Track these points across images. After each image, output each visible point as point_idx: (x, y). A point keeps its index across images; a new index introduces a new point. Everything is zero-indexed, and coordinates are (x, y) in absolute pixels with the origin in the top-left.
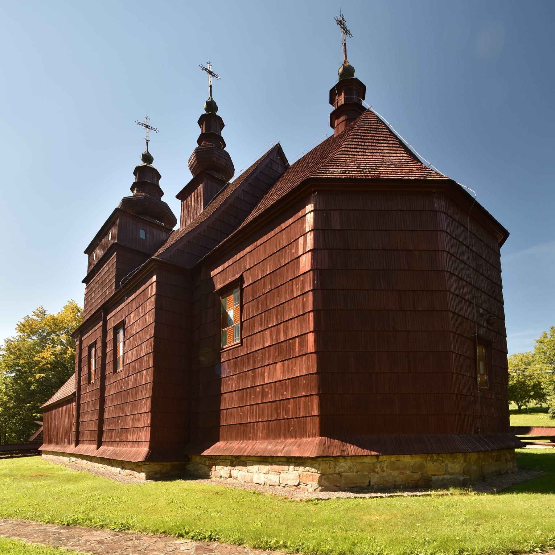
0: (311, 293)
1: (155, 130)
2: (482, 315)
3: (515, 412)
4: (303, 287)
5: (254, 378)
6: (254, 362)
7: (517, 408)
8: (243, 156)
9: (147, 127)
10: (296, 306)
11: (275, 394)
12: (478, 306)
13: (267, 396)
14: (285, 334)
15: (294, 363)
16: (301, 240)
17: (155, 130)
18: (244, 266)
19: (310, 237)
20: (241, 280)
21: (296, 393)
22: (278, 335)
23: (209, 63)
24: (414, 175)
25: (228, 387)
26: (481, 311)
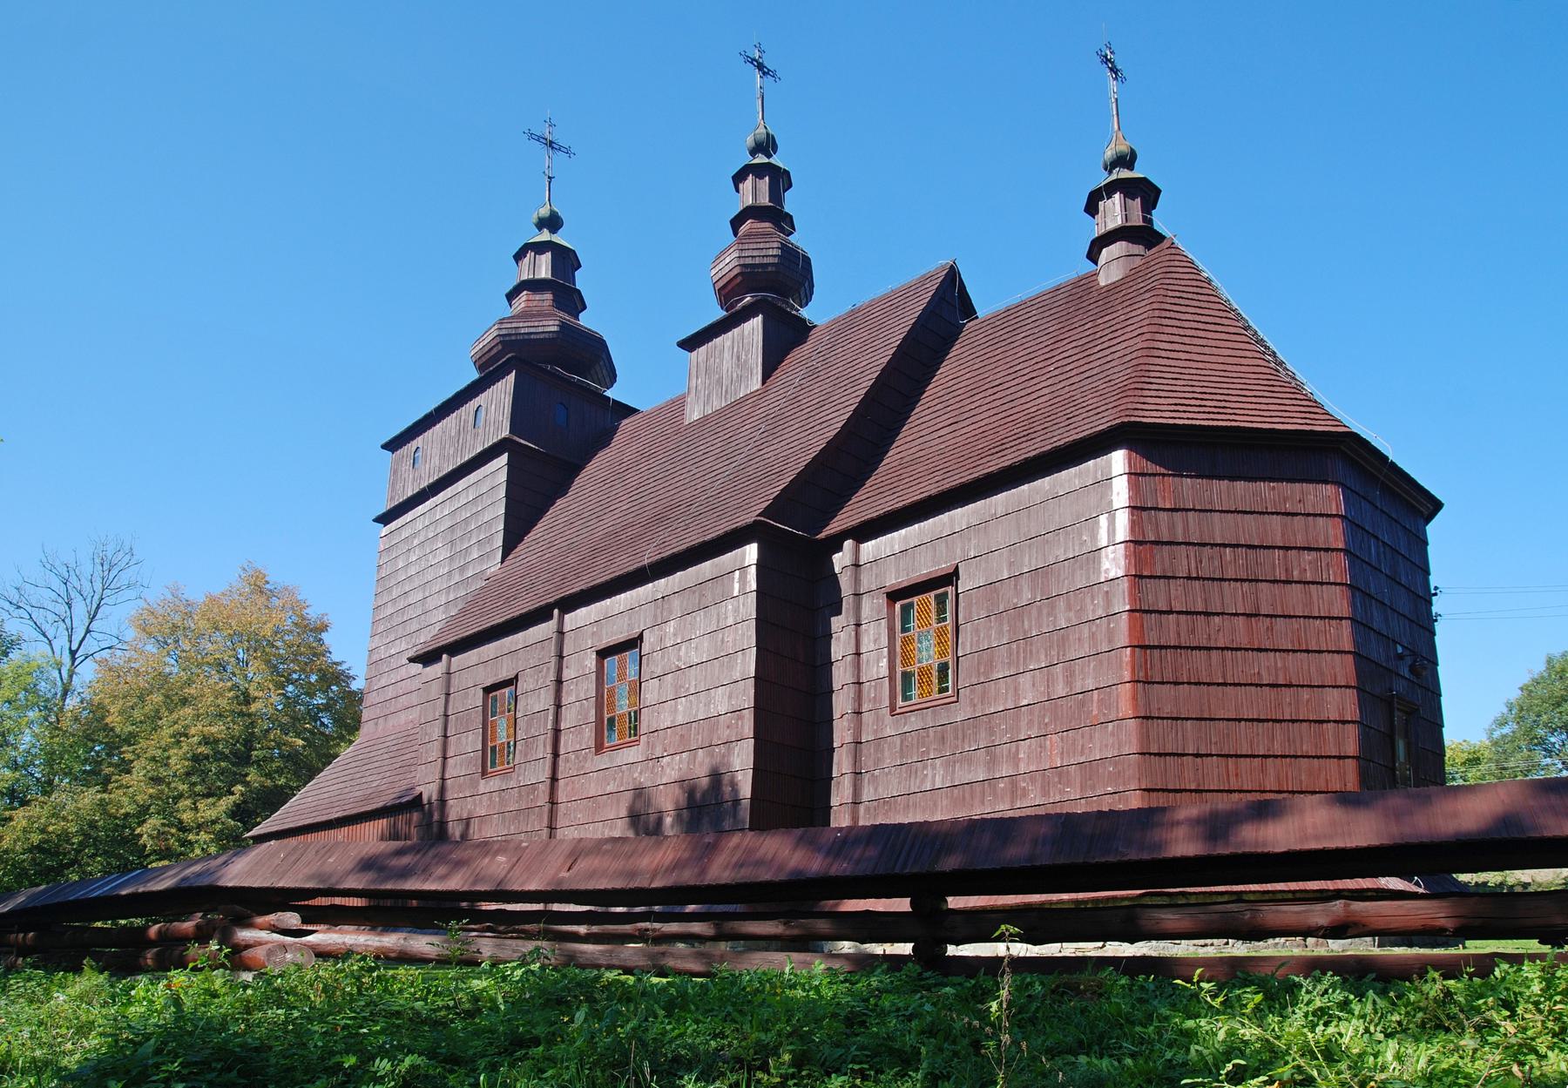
0: (1125, 616)
1: (531, 136)
2: (1400, 657)
3: (855, 818)
4: (1108, 603)
5: (992, 762)
6: (991, 732)
7: (865, 798)
8: (858, 280)
9: (551, 144)
10: (1093, 636)
11: (1045, 793)
12: (1395, 642)
13: (1025, 793)
14: (1069, 682)
15: (1087, 736)
16: (1103, 520)
17: (531, 136)
18: (963, 550)
19: (1123, 519)
20: (951, 578)
21: (1093, 788)
22: (1050, 682)
23: (758, 47)
24: (1293, 423)
25: (923, 781)
26: (1400, 650)
